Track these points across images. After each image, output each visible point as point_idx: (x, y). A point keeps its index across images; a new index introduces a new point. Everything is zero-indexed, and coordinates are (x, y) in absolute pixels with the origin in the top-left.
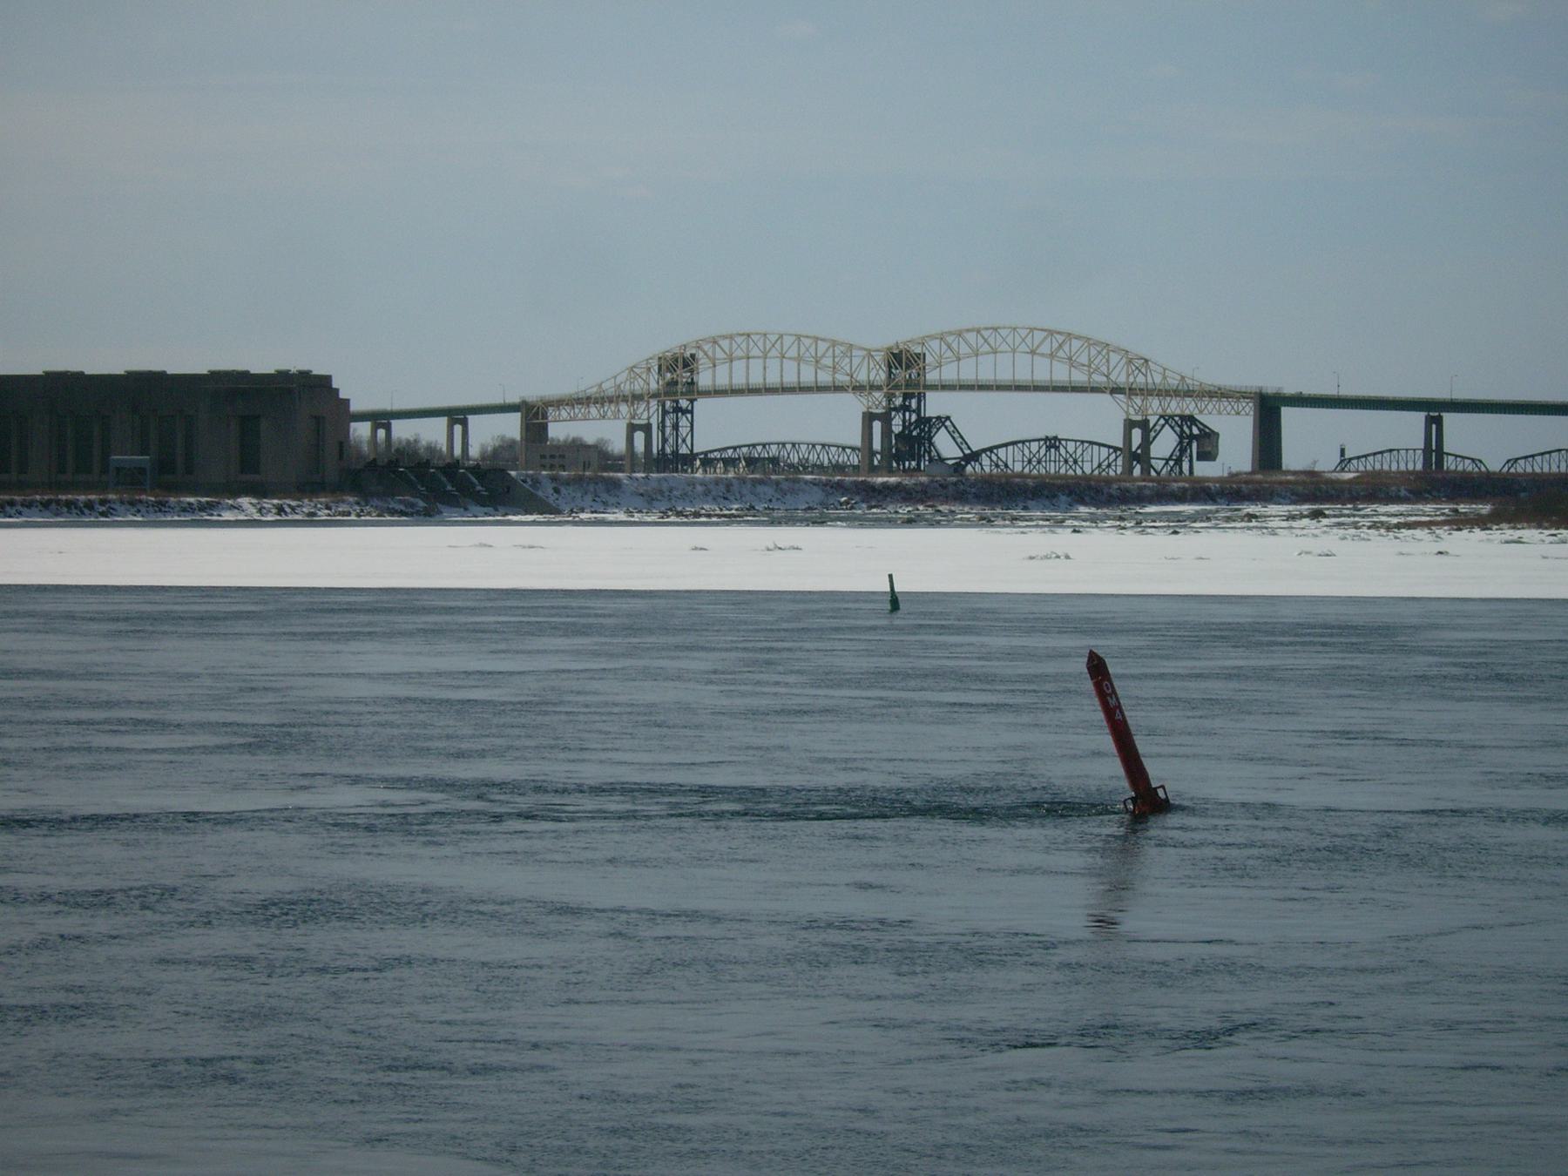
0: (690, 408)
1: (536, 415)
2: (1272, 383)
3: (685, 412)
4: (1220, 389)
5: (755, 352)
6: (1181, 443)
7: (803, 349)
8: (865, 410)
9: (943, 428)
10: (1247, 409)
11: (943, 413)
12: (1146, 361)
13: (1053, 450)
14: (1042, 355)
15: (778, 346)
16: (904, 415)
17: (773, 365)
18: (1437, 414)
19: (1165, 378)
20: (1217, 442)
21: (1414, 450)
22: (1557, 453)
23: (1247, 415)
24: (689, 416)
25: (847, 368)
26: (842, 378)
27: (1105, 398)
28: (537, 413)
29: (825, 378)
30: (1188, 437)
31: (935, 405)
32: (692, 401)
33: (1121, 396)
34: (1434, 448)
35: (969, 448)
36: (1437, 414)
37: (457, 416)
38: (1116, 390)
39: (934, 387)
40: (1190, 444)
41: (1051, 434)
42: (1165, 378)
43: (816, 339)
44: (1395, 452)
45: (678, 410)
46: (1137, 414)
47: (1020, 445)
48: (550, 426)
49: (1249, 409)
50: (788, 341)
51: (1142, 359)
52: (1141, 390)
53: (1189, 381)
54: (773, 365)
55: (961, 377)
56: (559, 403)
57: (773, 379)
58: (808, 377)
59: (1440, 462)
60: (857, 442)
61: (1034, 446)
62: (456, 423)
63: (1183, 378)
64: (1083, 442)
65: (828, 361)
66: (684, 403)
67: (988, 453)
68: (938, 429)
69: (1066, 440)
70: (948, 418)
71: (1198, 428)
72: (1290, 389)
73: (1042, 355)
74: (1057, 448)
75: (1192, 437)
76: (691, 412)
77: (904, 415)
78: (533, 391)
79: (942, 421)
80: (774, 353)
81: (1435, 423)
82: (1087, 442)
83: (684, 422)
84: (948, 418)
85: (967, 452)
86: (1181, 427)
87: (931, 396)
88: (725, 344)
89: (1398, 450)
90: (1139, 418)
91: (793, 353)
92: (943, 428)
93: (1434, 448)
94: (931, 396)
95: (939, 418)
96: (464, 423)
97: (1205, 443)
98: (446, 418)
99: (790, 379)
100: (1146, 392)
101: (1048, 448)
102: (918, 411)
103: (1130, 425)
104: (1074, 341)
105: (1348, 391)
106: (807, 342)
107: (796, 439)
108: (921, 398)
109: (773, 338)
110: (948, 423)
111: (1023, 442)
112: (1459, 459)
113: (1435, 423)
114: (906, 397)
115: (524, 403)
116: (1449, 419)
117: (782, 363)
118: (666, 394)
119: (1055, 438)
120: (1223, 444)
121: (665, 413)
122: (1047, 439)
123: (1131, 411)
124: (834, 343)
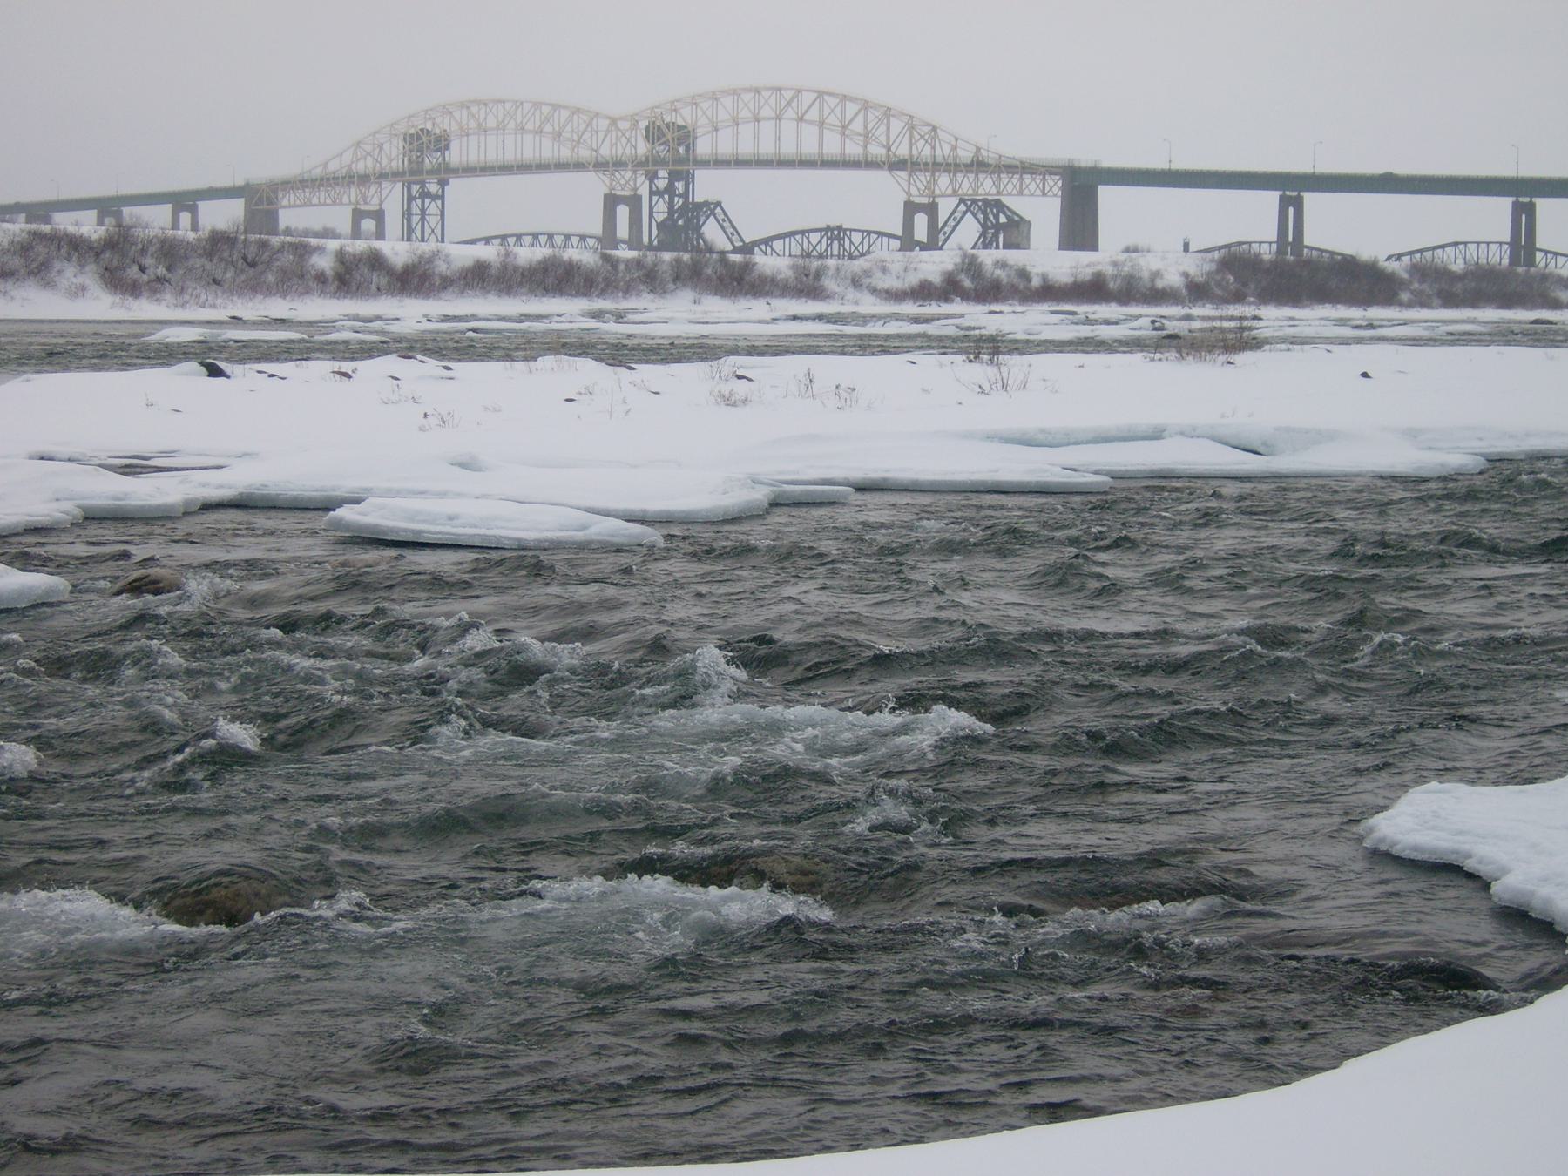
0: (655, 198)
1: (260, 200)
2: (1085, 156)
3: (434, 197)
4: (1022, 163)
5: (766, 112)
6: (984, 234)
7: (838, 111)
8: (607, 191)
9: (712, 218)
10: (1055, 189)
11: (712, 198)
12: (934, 129)
13: (836, 242)
14: (811, 122)
15: (794, 104)
16: (423, 203)
17: (788, 127)
18: (1295, 194)
19: (954, 148)
20: (1029, 233)
21: (1488, 243)
22: (1453, 248)
23: (1055, 195)
24: (439, 202)
25: (883, 139)
26: (876, 151)
27: (883, 175)
28: (260, 199)
29: (854, 150)
30: (993, 226)
31: (706, 186)
32: (443, 183)
33: (903, 174)
34: (1290, 239)
35: (742, 240)
36: (1295, 194)
37: (184, 201)
38: (897, 165)
39: (705, 164)
40: (996, 235)
41: (833, 224)
42: (954, 148)
43: (844, 98)
44: (1461, 246)
45: (425, 195)
46: (921, 195)
47: (798, 237)
48: (281, 212)
49: (1055, 184)
50: (808, 98)
51: (929, 125)
52: (926, 164)
53: (984, 153)
54: (788, 127)
55: (761, 151)
56: (287, 185)
57: (788, 149)
58: (832, 147)
59: (1530, 262)
60: (598, 230)
61: (814, 238)
62: (182, 210)
63: (978, 149)
64: (869, 233)
65: (857, 126)
66: (433, 188)
67: (763, 247)
68: (708, 217)
69: (851, 230)
70: (719, 204)
71: (1007, 217)
72: (1107, 162)
73: (811, 122)
74: (840, 240)
75: (998, 227)
76: (442, 198)
77: (423, 203)
78: (261, 171)
79: (711, 208)
80: (790, 113)
81: (1524, 215)
82: (874, 232)
83: (433, 208)
84: (719, 204)
85: (738, 244)
86: (985, 213)
87: (701, 175)
88: (728, 101)
89: (1465, 243)
90: (925, 200)
91: (813, 115)
92: (712, 218)
93: (1290, 239)
94: (701, 175)
95: (706, 204)
96: (1298, 204)
97: (1012, 231)
98: (95, 211)
99: (810, 149)
100: (934, 166)
101: (832, 239)
102: (685, 195)
103: (911, 209)
104: (562, 111)
105: (1181, 164)
106: (832, 101)
107: (551, 229)
108: (688, 178)
109: (788, 95)
110: (718, 210)
111: (802, 232)
112: (1550, 256)
113: (1524, 215)
114: (674, 177)
115: (247, 186)
116: (1311, 200)
117: (806, 121)
118: (412, 173)
119: (839, 228)
120: (1035, 235)
121: (411, 199)
122: (828, 229)
123: (914, 191)
124: (866, 106)
